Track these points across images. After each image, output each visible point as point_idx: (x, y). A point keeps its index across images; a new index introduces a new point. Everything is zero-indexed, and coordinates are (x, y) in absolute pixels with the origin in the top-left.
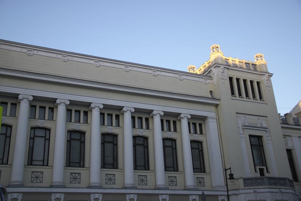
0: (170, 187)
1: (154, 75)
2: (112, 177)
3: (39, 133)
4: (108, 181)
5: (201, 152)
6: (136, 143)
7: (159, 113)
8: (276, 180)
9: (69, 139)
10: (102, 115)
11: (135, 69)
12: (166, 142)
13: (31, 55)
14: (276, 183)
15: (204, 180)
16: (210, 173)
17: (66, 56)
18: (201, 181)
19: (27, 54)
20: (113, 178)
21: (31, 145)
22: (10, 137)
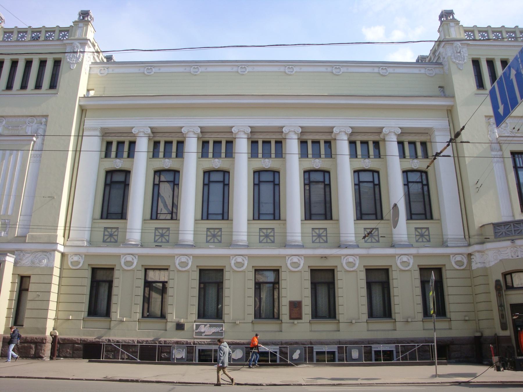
0: (415, 244)
2: (425, 232)
3: (265, 177)
4: (264, 239)
5: (377, 187)
6: (361, 180)
7: (293, 130)
9: (357, 182)
10: (401, 145)
12: (409, 174)
16: (338, 220)
18: (159, 233)
20: (427, 233)
22: (279, 185)
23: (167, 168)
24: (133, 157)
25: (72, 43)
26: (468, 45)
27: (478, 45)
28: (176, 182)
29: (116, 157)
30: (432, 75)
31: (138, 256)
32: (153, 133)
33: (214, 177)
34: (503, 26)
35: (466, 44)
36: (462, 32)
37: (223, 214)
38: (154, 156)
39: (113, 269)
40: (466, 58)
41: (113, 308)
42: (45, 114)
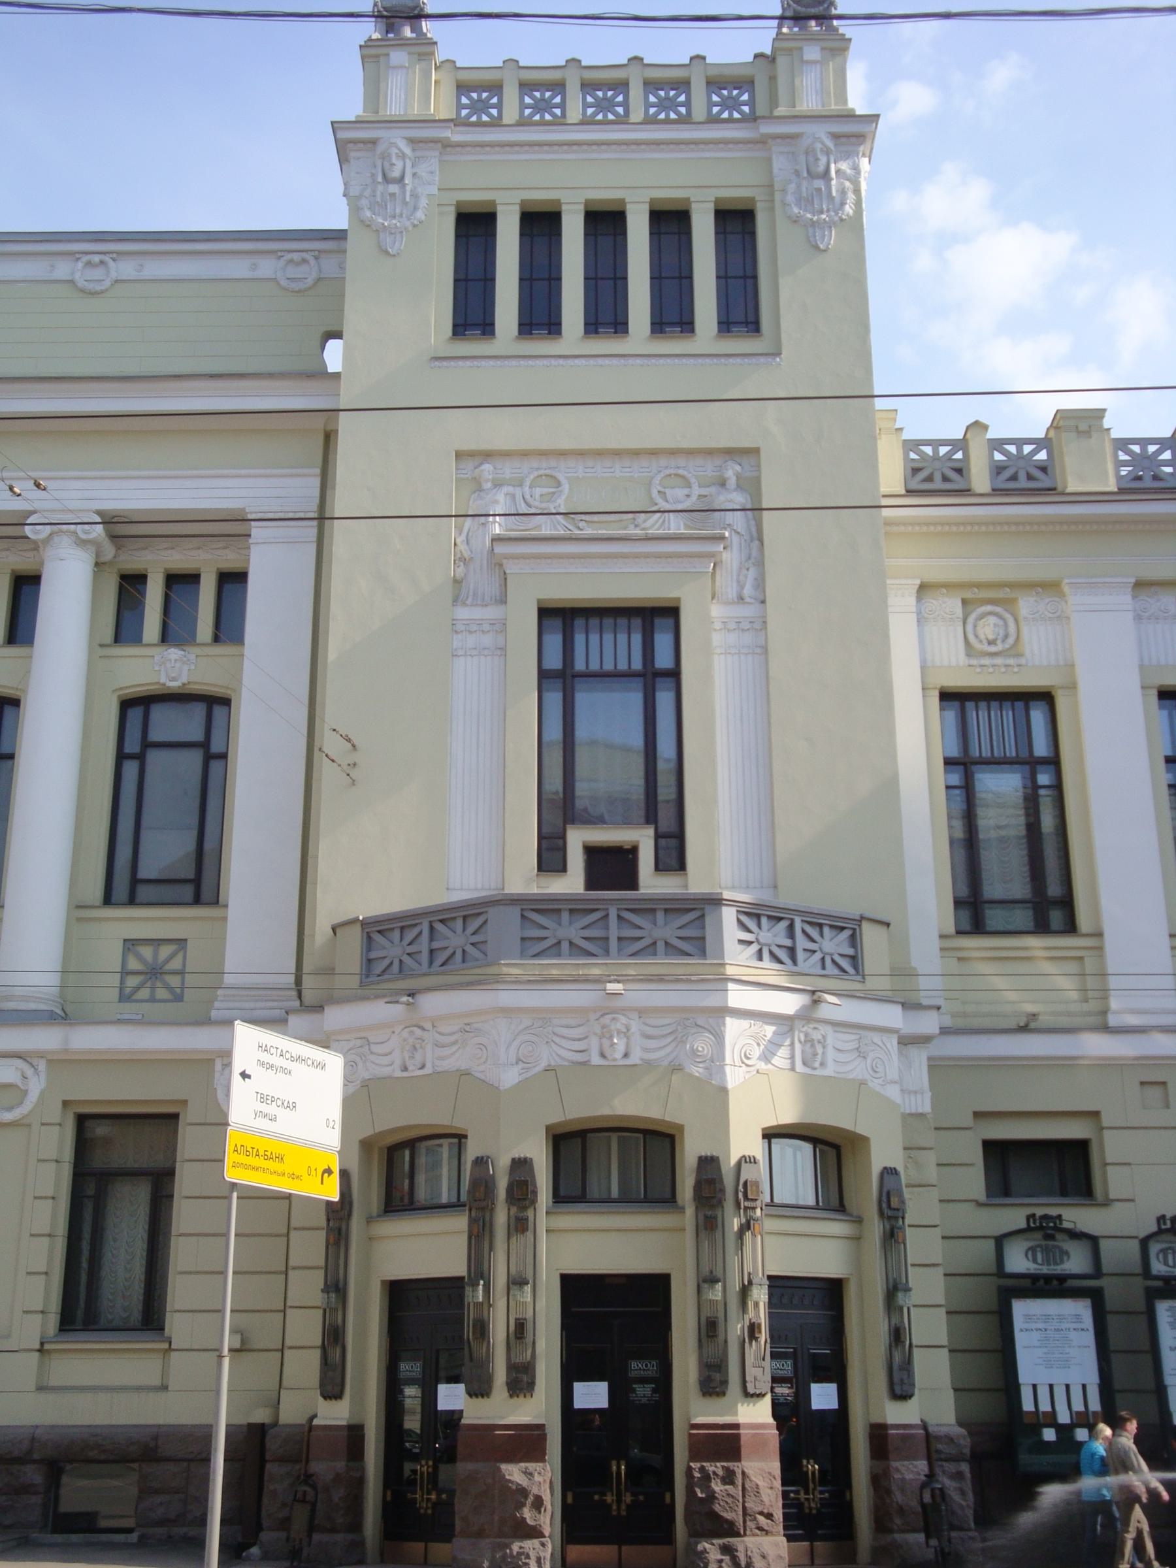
1: (295, 286)
8: (791, 927)
11: (156, 269)
13: (98, 288)
14: (792, 951)
15: (185, 957)
17: (106, 258)
19: (284, 283)
21: (555, 783)
23: (174, 685)
24: (29, 641)
25: (374, 142)
26: (446, 145)
27: (491, 145)
28: (216, 747)
29: (165, 637)
30: (301, 286)
31: (49, 1062)
32: (113, 537)
33: (168, 724)
34: (637, 59)
35: (435, 141)
36: (448, 90)
37: (197, 882)
38: (118, 639)
39: (173, 1118)
40: (423, 202)
41: (180, 1292)
42: (746, 444)
